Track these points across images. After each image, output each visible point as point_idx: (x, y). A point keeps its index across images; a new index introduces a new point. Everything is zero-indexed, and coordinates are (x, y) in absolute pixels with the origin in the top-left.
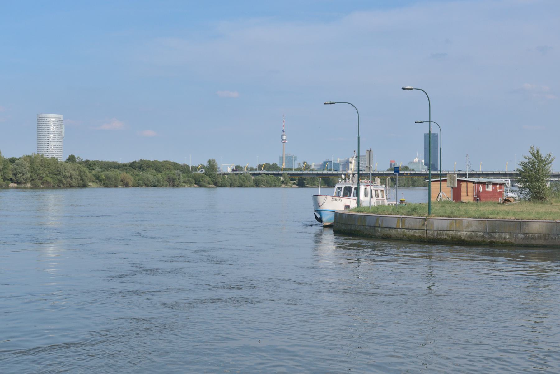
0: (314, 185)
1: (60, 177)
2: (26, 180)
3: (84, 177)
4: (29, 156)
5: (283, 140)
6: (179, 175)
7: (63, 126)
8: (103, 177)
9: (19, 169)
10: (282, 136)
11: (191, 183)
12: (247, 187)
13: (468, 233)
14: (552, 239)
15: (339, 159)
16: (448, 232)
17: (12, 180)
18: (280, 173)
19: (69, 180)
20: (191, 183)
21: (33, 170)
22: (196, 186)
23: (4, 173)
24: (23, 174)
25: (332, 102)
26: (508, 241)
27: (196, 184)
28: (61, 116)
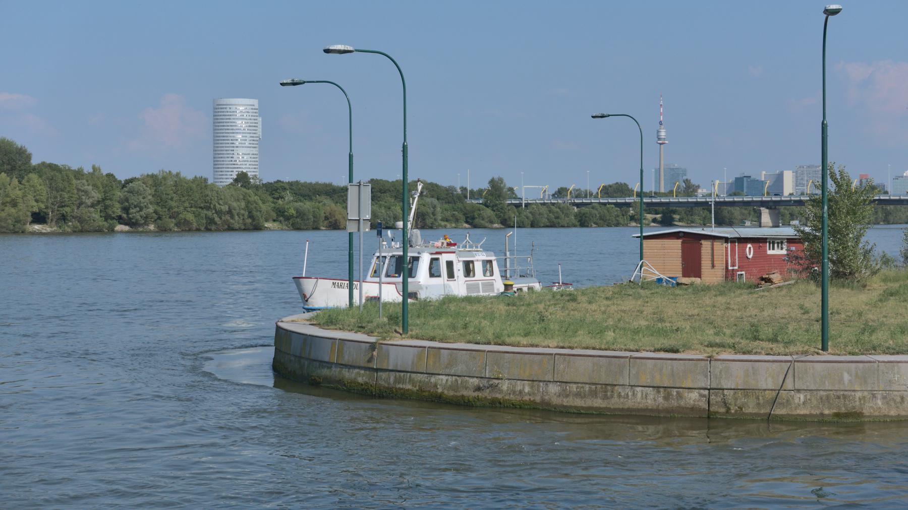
0: (692, 222)
1: (209, 213)
2: (146, 217)
3: (255, 213)
4: (153, 176)
5: (659, 139)
6: (434, 207)
7: (260, 119)
8: (292, 211)
9: (134, 200)
10: (658, 132)
11: (457, 220)
12: (563, 226)
13: (450, 378)
14: (619, 396)
15: (764, 172)
16: (413, 375)
17: (120, 220)
18: (628, 200)
19: (228, 217)
20: (457, 220)
21: (160, 200)
22: (467, 226)
23: (106, 207)
24: (141, 210)
25: (296, 80)
26: (527, 398)
27: (467, 222)
28: (255, 102)
